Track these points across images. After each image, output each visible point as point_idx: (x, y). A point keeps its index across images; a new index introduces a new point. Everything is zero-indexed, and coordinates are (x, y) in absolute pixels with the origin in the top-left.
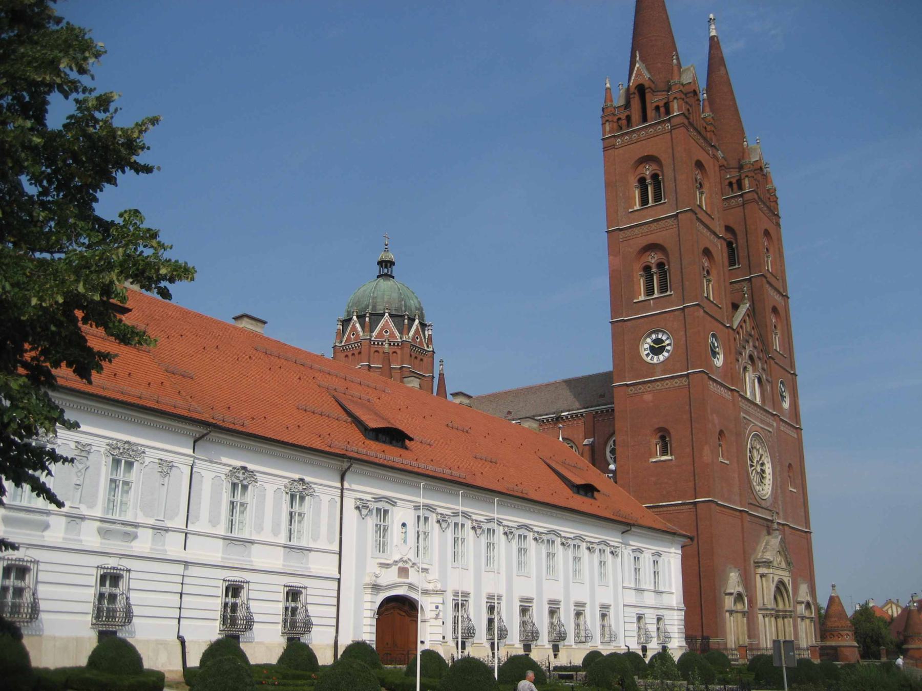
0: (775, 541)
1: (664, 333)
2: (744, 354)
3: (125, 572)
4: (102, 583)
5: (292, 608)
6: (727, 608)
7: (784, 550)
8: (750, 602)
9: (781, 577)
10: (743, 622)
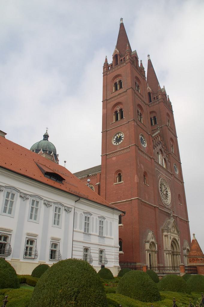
0: (172, 220)
1: (121, 133)
2: (157, 147)
4: (27, 244)
5: (86, 254)
6: (146, 249)
7: (176, 226)
8: (159, 247)
9: (175, 237)
10: (155, 256)
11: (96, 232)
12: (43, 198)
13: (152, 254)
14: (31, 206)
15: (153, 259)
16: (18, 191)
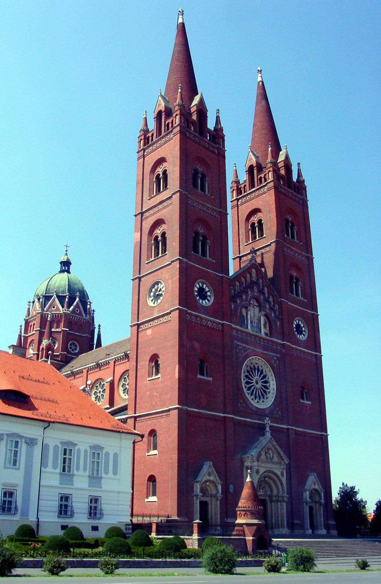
15: (212, 510)
16: (21, 437)
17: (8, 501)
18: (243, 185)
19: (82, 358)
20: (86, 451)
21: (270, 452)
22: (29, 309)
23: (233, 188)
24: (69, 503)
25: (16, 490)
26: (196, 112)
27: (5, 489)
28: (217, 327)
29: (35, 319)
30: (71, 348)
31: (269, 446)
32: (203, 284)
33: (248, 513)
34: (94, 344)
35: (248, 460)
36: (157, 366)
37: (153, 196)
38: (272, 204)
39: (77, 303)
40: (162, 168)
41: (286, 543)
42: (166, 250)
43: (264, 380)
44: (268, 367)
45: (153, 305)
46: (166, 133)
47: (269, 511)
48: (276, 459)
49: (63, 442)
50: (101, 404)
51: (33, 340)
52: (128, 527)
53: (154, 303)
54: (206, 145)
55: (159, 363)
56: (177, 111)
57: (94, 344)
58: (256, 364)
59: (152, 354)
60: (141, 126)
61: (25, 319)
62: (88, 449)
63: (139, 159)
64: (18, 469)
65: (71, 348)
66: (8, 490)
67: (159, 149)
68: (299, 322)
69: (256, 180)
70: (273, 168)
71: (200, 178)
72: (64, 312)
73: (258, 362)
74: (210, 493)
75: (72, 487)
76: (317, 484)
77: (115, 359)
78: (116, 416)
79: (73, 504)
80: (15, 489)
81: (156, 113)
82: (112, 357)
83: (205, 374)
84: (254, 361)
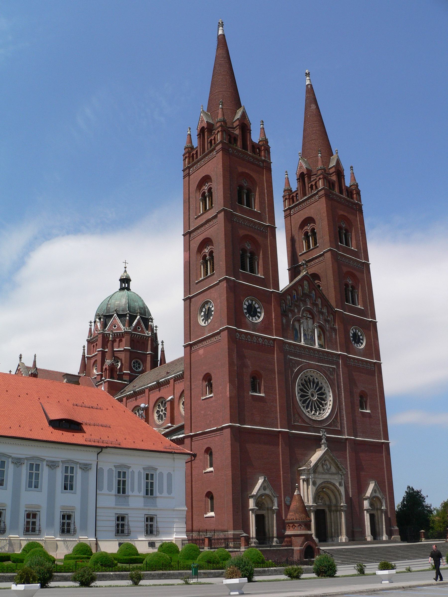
3: (3, 510)
4: (147, 521)
6: (365, 508)
11: (139, 491)
12: (11, 455)
13: (268, 514)
14: (29, 471)
16: (77, 463)
17: (121, 524)
18: (296, 193)
19: (145, 377)
20: (139, 473)
21: (327, 463)
22: (91, 329)
23: (285, 197)
24: (126, 522)
25: (73, 513)
26: (238, 127)
27: (64, 512)
28: (269, 343)
29: (97, 339)
30: (134, 366)
31: (326, 457)
32: (252, 301)
33: (295, 525)
34: (158, 361)
35: (305, 473)
36: (210, 385)
37: (199, 214)
38: (324, 213)
39: (139, 321)
40: (207, 186)
41: (337, 550)
42: (214, 269)
43: (320, 392)
44: (323, 378)
45: (204, 325)
46: (208, 150)
47: (328, 521)
48: (333, 470)
49: (116, 466)
50: (164, 422)
51: (96, 361)
52: (184, 542)
53: (205, 323)
54: (251, 159)
55: (211, 382)
56: (218, 128)
57: (158, 361)
58: (311, 376)
59: (205, 373)
60: (184, 143)
61: (87, 340)
62: (142, 471)
63: (184, 177)
64: (75, 493)
65: (134, 366)
66: (66, 513)
67: (204, 166)
68: (356, 331)
69: (307, 188)
70: (323, 175)
71: (246, 193)
72: (125, 331)
73: (313, 374)
74: (266, 506)
75: (128, 507)
76: (378, 491)
77: (175, 377)
78: (174, 435)
79: (130, 523)
80: (73, 512)
81: (199, 130)
82: (172, 375)
83: (258, 390)
84: (309, 374)
